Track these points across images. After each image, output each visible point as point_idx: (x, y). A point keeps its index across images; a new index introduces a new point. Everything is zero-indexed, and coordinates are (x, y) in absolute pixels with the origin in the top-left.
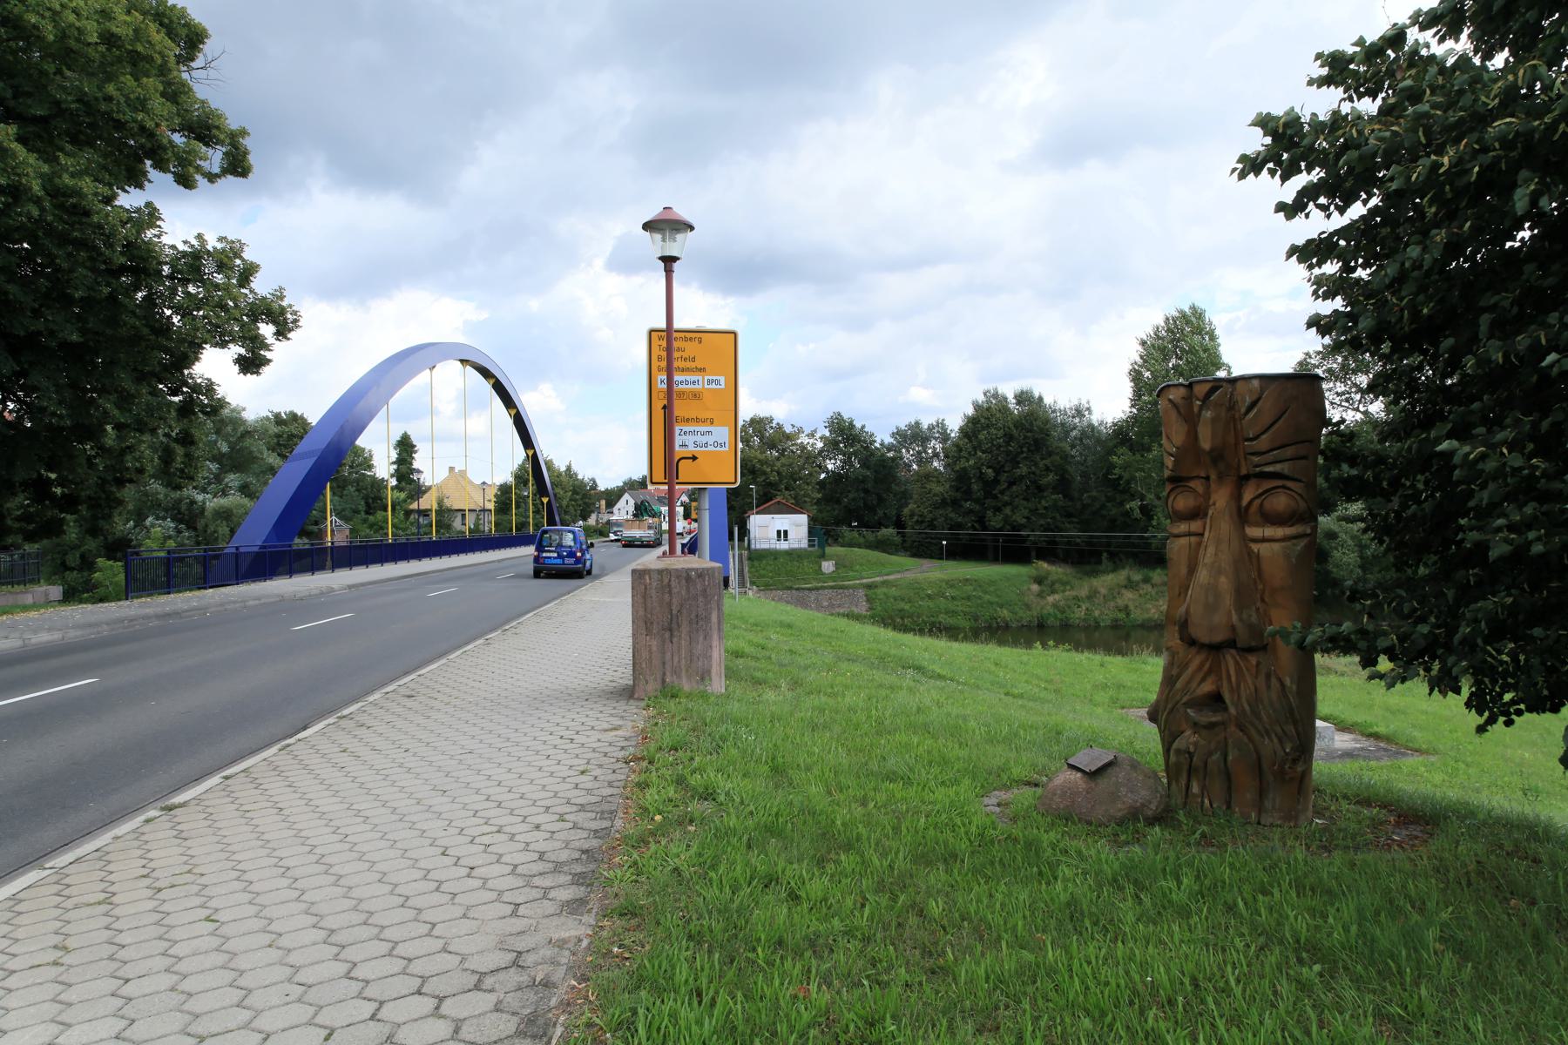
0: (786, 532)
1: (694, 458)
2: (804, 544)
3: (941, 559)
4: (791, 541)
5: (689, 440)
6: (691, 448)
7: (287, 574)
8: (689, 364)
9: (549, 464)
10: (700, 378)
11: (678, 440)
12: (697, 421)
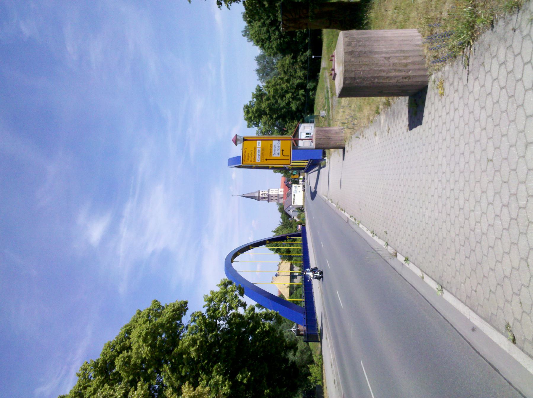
0: (307, 134)
1: (283, 151)
2: (312, 125)
3: (321, 58)
4: (311, 131)
5: (277, 152)
6: (279, 151)
7: (312, 294)
8: (253, 152)
9: (277, 231)
10: (257, 148)
11: (277, 155)
12: (271, 149)
